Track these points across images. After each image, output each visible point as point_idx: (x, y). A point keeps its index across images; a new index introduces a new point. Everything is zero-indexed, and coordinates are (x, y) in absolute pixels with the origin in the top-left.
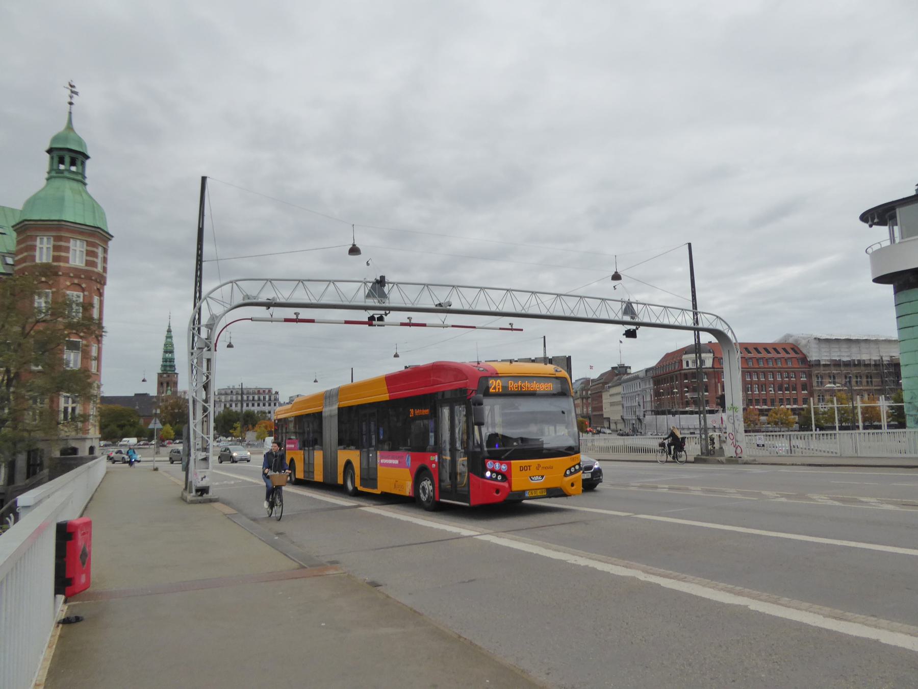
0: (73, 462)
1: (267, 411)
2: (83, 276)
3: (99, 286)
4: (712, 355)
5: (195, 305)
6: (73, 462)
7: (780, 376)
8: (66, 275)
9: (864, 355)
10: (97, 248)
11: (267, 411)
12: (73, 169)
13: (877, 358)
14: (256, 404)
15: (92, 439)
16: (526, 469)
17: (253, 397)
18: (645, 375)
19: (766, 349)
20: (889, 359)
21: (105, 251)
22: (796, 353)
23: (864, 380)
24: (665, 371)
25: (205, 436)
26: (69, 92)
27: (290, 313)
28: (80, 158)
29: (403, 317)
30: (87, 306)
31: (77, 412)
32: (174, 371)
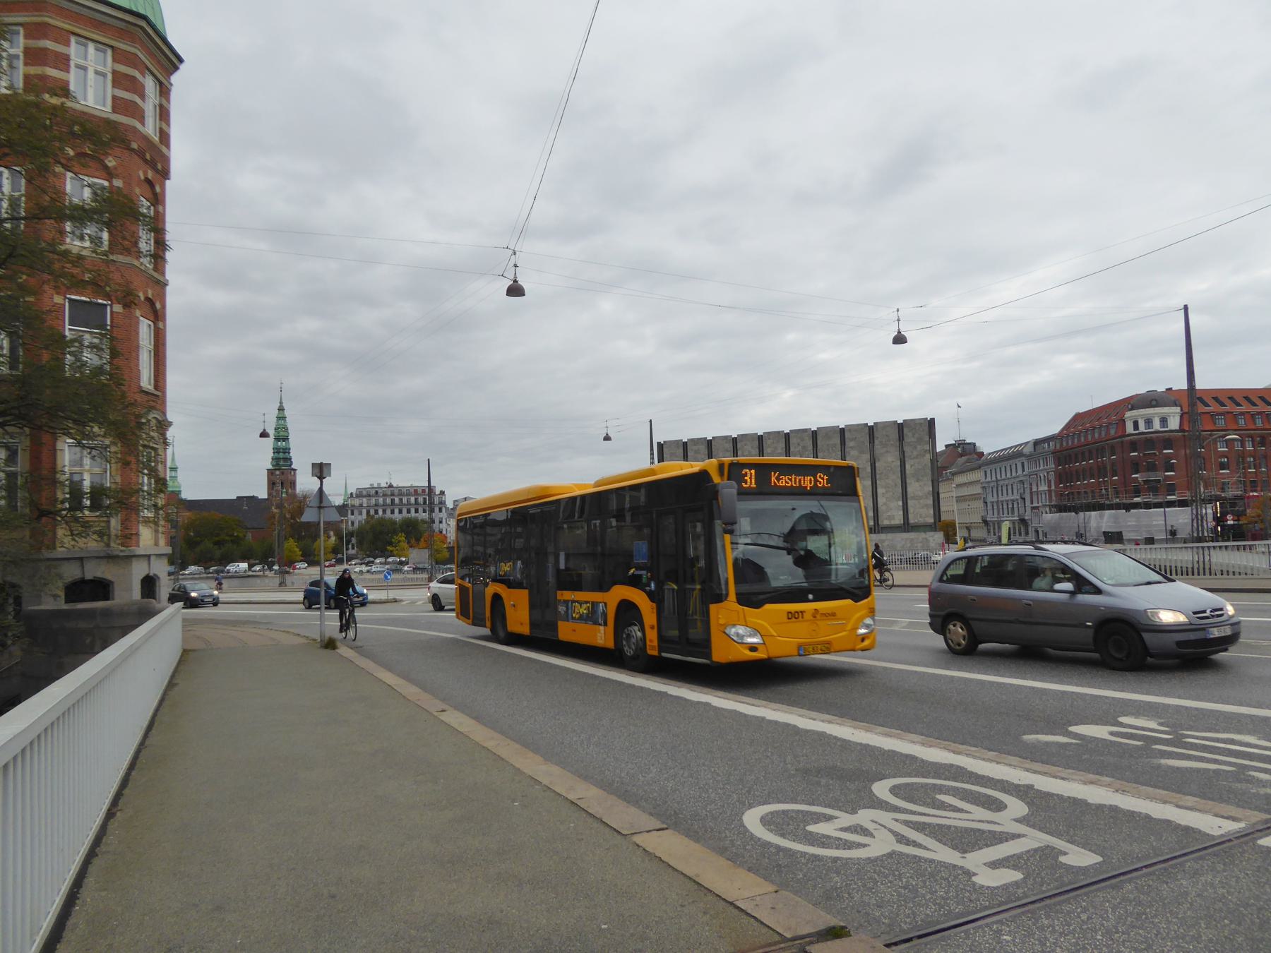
0: (82, 625)
4: (1178, 410)
6: (82, 625)
7: (1251, 443)
14: (396, 511)
15: (149, 557)
17: (416, 499)
18: (1033, 450)
21: (164, 91)
24: (1070, 443)
32: (290, 465)
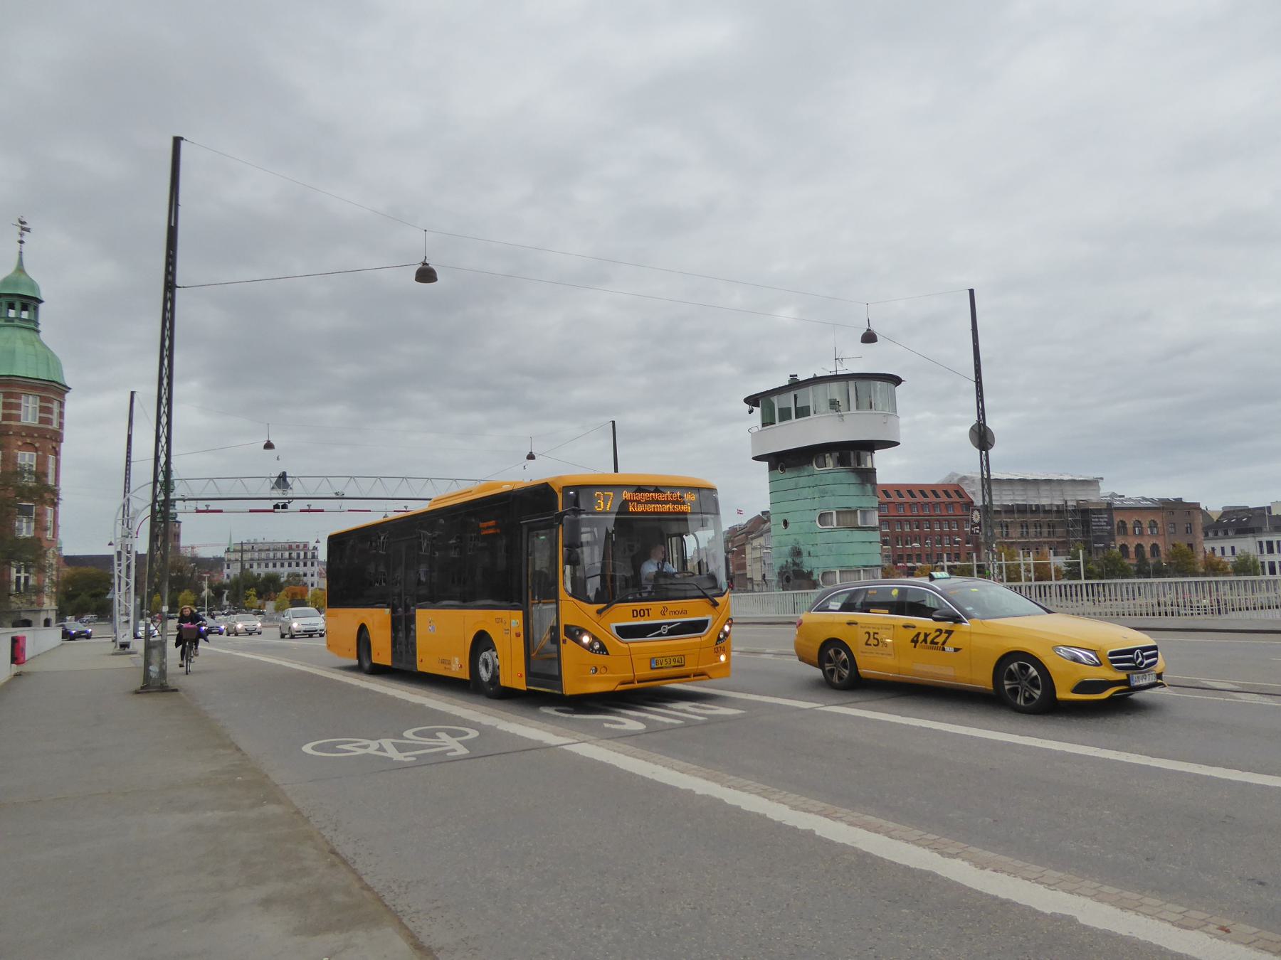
1: (301, 573)
2: (36, 435)
3: (54, 444)
5: (125, 496)
8: (18, 434)
9: (1045, 499)
10: (52, 404)
11: (301, 573)
12: (25, 315)
13: (1060, 503)
14: (286, 564)
15: (47, 610)
16: (642, 614)
17: (290, 554)
19: (922, 492)
20: (1075, 504)
21: (62, 405)
22: (961, 496)
23: (1045, 530)
25: (127, 605)
26: (19, 230)
27: (202, 506)
28: (33, 303)
29: (303, 504)
30: (40, 475)
31: (31, 582)
